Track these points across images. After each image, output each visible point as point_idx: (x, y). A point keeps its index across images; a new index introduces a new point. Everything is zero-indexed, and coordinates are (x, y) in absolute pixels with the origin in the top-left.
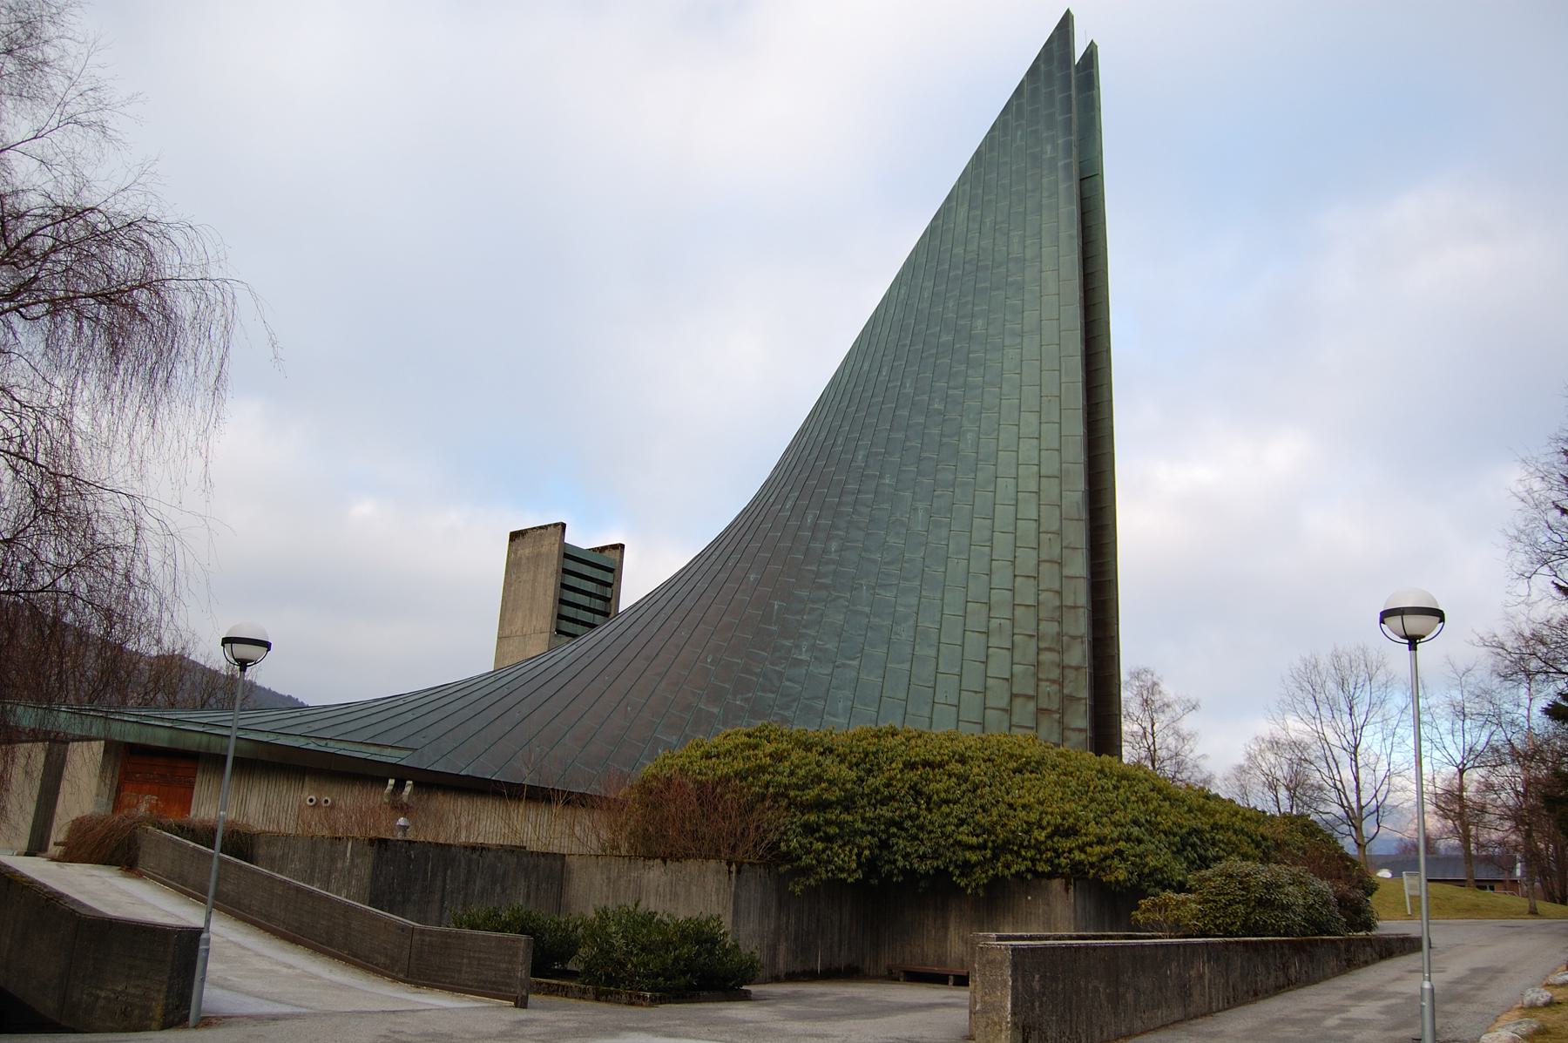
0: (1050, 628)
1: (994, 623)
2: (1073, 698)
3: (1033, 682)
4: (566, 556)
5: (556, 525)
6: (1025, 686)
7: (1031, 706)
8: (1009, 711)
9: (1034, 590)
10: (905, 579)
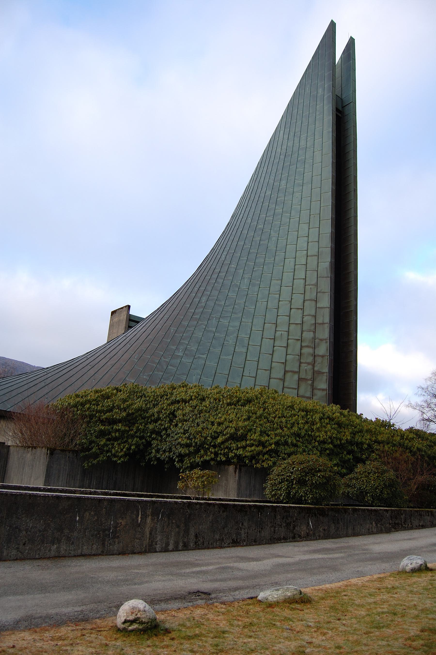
0: (308, 335)
1: (278, 333)
2: (320, 373)
3: (298, 364)
4: (130, 320)
5: (126, 306)
6: (293, 366)
7: (296, 377)
8: (283, 380)
9: (301, 315)
10: (235, 313)
